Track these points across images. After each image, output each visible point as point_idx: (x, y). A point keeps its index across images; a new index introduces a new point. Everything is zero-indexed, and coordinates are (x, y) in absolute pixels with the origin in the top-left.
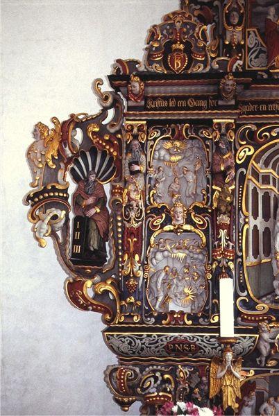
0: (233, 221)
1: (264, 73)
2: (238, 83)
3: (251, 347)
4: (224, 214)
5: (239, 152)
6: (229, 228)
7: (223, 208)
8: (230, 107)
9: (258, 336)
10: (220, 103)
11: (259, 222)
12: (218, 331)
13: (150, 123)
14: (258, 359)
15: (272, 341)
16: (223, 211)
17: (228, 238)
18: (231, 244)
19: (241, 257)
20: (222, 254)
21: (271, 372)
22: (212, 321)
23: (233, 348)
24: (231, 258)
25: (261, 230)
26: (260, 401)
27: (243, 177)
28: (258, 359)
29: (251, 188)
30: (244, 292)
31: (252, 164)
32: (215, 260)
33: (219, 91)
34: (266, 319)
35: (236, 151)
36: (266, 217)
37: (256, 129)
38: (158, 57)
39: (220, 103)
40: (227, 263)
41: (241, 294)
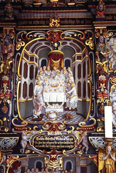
0: (11, 80)
1: (31, 5)
2: (14, 9)
3: (15, 144)
4: (6, 75)
5: (17, 44)
6: (9, 83)
7: (5, 73)
8: (12, 21)
9: (18, 138)
10: (6, 19)
11: (28, 80)
12: (104, 135)
13: (108, 28)
15: (28, 140)
16: (5, 74)
17: (8, 88)
18: (9, 91)
19: (16, 98)
20: (4, 96)
21: (27, 156)
22: (97, 131)
24: (8, 98)
25: (28, 84)
27: (19, 57)
29: (24, 63)
30: (16, 115)
31: (24, 50)
33: (5, 12)
34: (27, 129)
35: (16, 44)
36: (31, 78)
37: (26, 33)
39: (6, 19)
40: (7, 100)
41: (15, 116)
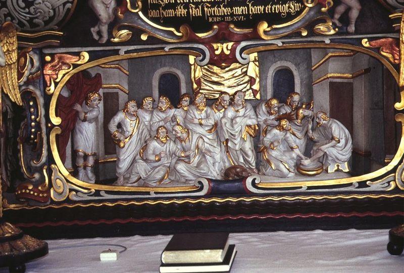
14: (94, 30)
21: (122, 52)
23: (32, 9)
26: (111, 108)
28: (94, 30)
32: (64, 64)
38: (9, 227)
